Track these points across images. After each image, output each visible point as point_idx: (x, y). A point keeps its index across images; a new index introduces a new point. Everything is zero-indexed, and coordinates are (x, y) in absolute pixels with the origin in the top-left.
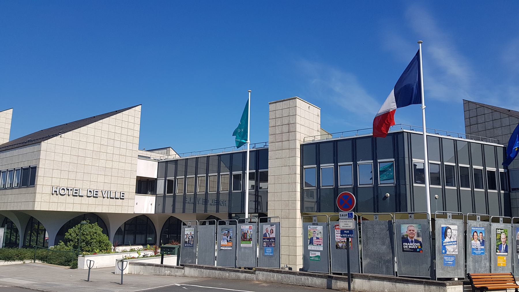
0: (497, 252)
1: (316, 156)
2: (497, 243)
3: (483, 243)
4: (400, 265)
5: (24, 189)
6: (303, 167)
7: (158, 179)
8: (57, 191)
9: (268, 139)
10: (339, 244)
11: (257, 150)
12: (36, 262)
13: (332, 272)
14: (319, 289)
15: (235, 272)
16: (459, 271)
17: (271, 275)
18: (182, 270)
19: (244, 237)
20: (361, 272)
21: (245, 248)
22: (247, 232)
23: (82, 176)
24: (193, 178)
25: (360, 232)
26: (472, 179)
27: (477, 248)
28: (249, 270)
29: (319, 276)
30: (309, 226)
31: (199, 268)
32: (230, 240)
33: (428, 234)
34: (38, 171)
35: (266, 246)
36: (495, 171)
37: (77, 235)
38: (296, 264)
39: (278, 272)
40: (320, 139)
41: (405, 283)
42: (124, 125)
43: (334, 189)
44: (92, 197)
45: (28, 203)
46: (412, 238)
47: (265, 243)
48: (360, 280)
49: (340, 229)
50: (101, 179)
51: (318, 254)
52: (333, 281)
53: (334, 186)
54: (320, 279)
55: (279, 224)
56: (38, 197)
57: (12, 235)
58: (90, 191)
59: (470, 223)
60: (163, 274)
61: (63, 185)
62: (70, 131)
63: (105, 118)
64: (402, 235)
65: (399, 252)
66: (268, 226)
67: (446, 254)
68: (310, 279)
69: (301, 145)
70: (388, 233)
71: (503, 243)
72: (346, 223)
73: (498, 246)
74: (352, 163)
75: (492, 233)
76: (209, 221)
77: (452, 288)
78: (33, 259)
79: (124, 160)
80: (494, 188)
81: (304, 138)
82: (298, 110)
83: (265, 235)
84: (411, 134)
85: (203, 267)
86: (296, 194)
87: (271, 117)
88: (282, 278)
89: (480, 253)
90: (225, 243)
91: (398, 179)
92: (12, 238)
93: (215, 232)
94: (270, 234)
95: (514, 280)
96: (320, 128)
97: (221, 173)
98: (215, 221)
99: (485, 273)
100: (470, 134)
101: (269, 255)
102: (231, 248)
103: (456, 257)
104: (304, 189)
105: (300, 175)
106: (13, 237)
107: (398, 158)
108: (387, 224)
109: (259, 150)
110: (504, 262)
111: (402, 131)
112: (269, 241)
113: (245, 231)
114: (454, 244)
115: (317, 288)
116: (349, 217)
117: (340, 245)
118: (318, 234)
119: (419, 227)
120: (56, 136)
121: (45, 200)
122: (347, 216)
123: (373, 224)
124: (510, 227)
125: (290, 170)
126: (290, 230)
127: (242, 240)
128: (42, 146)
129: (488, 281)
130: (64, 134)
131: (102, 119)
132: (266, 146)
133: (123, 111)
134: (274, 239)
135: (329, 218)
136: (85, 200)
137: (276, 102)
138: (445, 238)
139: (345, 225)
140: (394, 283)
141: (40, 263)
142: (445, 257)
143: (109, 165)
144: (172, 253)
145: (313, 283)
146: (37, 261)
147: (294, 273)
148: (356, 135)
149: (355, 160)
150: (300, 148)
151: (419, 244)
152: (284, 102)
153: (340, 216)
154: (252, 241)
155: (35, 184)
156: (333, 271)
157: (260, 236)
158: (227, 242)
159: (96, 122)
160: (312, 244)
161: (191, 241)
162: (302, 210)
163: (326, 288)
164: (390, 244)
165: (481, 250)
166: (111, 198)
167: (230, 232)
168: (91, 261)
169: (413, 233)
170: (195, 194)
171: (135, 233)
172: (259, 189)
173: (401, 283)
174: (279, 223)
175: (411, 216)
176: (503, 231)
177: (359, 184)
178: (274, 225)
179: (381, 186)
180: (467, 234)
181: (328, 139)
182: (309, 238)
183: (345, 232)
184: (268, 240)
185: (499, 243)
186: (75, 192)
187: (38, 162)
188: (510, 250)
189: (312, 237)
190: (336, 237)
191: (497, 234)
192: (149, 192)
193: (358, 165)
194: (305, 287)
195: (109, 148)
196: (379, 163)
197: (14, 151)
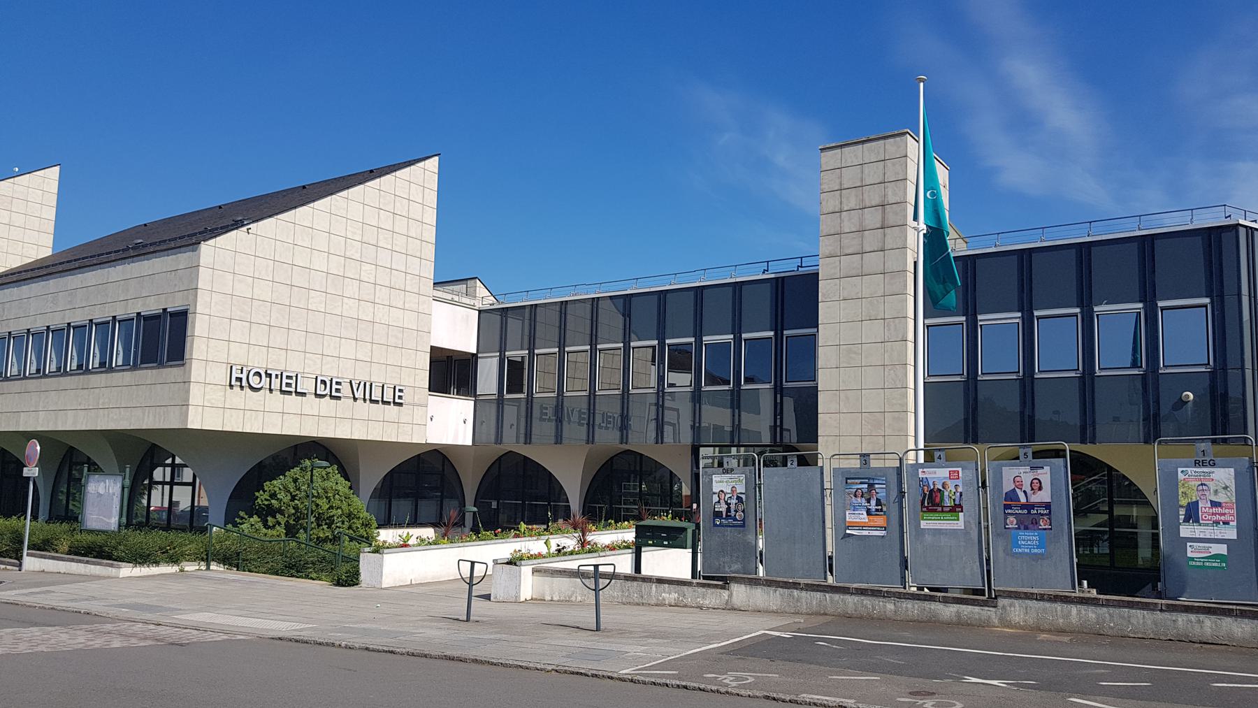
5: (150, 371)
7: (479, 355)
8: (241, 379)
9: (819, 245)
12: (212, 567)
15: (918, 600)
18: (722, 591)
22: (944, 488)
23: (303, 340)
24: (554, 355)
29: (1243, 615)
31: (781, 587)
32: (877, 510)
34: (194, 323)
35: (1016, 528)
37: (293, 498)
42: (401, 207)
43: (1022, 381)
44: (328, 398)
45: (165, 409)
50: (348, 350)
51: (1222, 549)
53: (1021, 374)
56: (196, 395)
57: (71, 498)
58: (324, 382)
60: (653, 601)
61: (256, 362)
62: (270, 216)
63: (355, 185)
66: (1022, 471)
68: (1182, 619)
74: (1077, 310)
76: (798, 456)
78: (202, 560)
79: (402, 303)
83: (1012, 496)
84: (1255, 232)
90: (864, 517)
92: (71, 507)
97: (599, 344)
98: (753, 456)
102: (882, 533)
106: (74, 503)
112: (1029, 513)
113: (934, 485)
120: (237, 228)
121: (213, 401)
125: (889, 330)
128: (202, 254)
130: (255, 225)
131: (348, 188)
132: (801, 267)
133: (395, 171)
134: (1047, 506)
136: (310, 403)
137: (841, 146)
141: (221, 572)
143: (366, 313)
144: (676, 543)
146: (214, 566)
149: (1085, 301)
154: (962, 511)
155: (187, 356)
158: (869, 512)
159: (332, 194)
161: (736, 511)
166: (372, 401)
167: (877, 486)
168: (473, 563)
170: (592, 396)
171: (416, 495)
172: (786, 382)
177: (1099, 369)
178: (1043, 468)
182: (1184, 502)
184: (1026, 512)
186: (287, 383)
187: (191, 298)
189: (1194, 500)
192: (454, 388)
193: (1097, 315)
195: (366, 267)
196: (1163, 309)
197: (110, 269)
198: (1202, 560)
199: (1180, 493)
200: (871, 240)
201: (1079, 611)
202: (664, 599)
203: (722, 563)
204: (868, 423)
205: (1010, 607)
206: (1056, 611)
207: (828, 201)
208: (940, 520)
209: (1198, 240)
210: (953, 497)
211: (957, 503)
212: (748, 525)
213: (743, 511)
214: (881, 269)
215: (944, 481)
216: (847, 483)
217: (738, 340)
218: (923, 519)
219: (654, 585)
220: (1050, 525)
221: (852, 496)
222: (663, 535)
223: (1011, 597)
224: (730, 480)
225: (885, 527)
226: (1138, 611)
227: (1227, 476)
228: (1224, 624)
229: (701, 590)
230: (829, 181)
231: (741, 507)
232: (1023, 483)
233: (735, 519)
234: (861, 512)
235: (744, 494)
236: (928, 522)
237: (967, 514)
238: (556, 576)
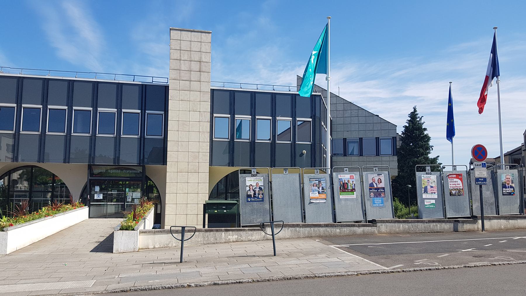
1: (231, 104)
10: (452, 191)
17: (396, 225)
21: (346, 200)
22: (348, 182)
31: (291, 227)
32: (322, 192)
35: (373, 197)
43: (250, 143)
51: (433, 201)
54: (448, 224)
60: (224, 241)
66: (375, 176)
72: (481, 172)
74: (271, 118)
85: (300, 225)
88: (409, 228)
90: (317, 195)
94: (377, 183)
98: (417, 166)
102: (325, 201)
104: (213, 140)
112: (378, 191)
116: (482, 167)
118: (432, 183)
122: (481, 166)
127: (341, 191)
134: (384, 188)
137: (181, 30)
139: (480, 174)
140: (508, 220)
149: (274, 115)
152: (193, 33)
154: (355, 191)
158: (319, 193)
161: (259, 194)
164: (493, 190)
167: (322, 182)
172: (147, 135)
173: (513, 219)
182: (423, 186)
183: (480, 179)
184: (376, 191)
189: (426, 186)
190: (450, 186)
199: (422, 183)
200: (194, 76)
202: (229, 239)
203: (252, 219)
204: (191, 156)
205: (381, 226)
208: (347, 195)
210: (352, 186)
211: (353, 188)
212: (265, 201)
213: (263, 194)
214: (199, 89)
215: (348, 179)
217: (19, 107)
218: (341, 195)
219: (223, 233)
220: (385, 195)
221: (312, 186)
222: (223, 207)
224: (255, 180)
225: (325, 199)
226: (420, 224)
228: (443, 225)
229: (250, 232)
230: (174, 45)
231: (261, 192)
232: (375, 180)
233: (258, 198)
235: (263, 186)
236: (343, 196)
237: (357, 192)
238: (157, 234)
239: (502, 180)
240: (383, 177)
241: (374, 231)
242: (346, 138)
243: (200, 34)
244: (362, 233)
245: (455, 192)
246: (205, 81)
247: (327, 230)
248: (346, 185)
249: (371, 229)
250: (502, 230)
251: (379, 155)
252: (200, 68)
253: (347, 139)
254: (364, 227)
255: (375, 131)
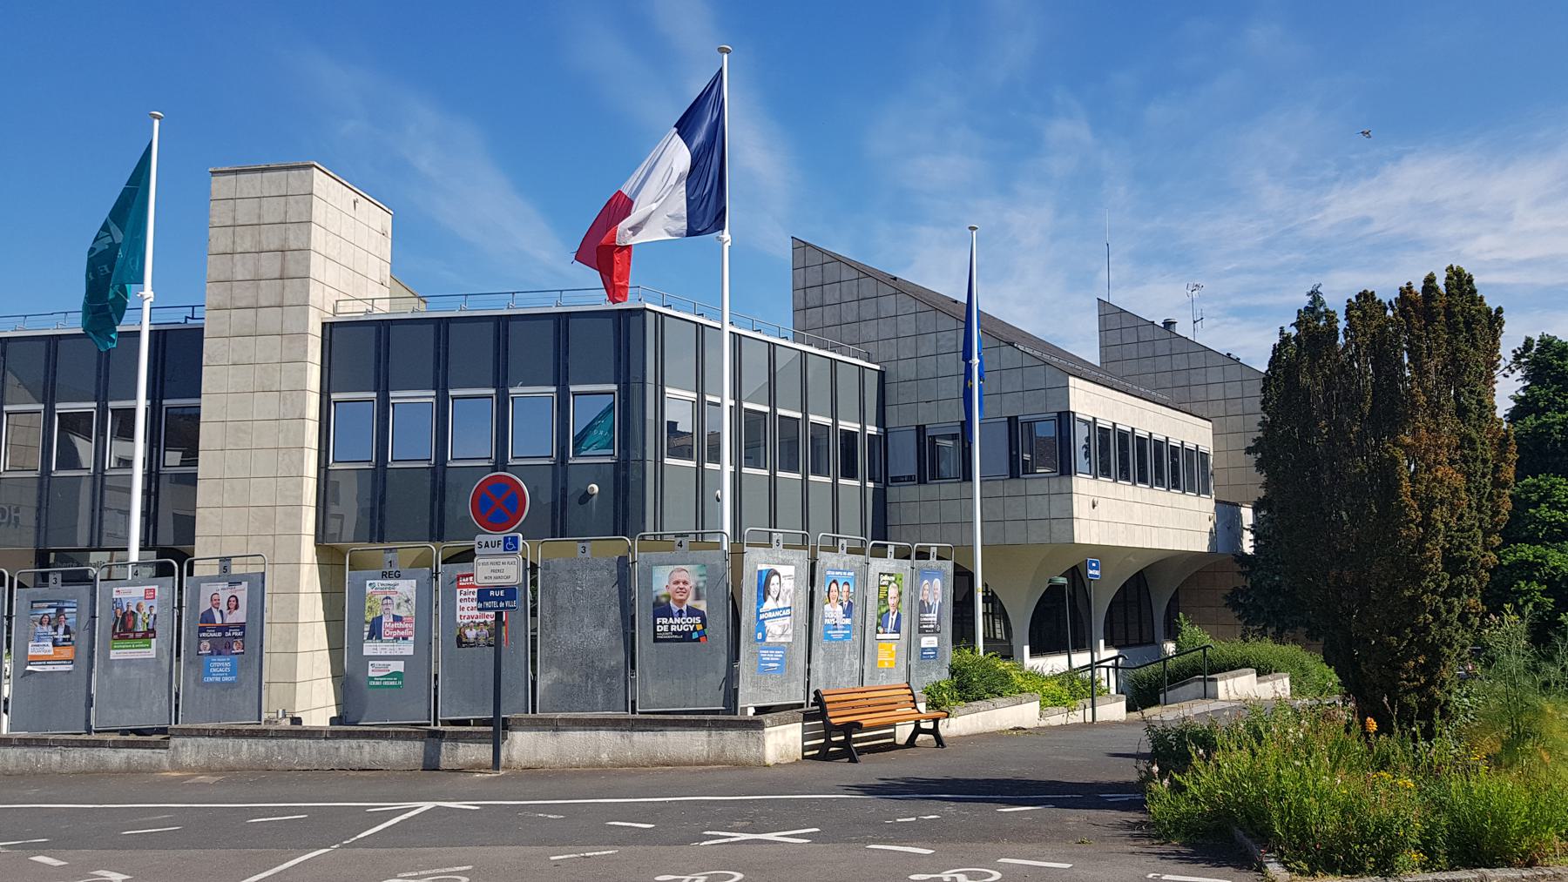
0: (878, 632)
2: (880, 608)
3: (848, 612)
4: (646, 682)
6: (329, 396)
11: (158, 331)
13: (440, 718)
14: (399, 773)
15: (87, 746)
16: (793, 686)
17: (228, 745)
19: (125, 627)
20: (530, 712)
22: (138, 610)
25: (534, 592)
26: (804, 451)
27: (836, 624)
28: (141, 736)
29: (398, 736)
30: (368, 582)
32: (64, 640)
33: (723, 588)
35: (210, 654)
36: (857, 430)
38: (294, 709)
39: (254, 734)
40: (386, 309)
41: (659, 729)
43: (433, 470)
46: (681, 602)
47: (206, 643)
48: (529, 733)
49: (476, 587)
51: (399, 666)
52: (445, 746)
55: (260, 578)
59: (825, 558)
64: (654, 595)
65: (643, 644)
66: (220, 587)
67: (764, 643)
68: (367, 746)
69: (324, 324)
70: (617, 592)
71: (892, 610)
72: (496, 567)
73: (880, 616)
74: (492, 391)
75: (870, 585)
77: (776, 732)
80: (853, 476)
81: (337, 301)
82: (317, 207)
83: (208, 617)
86: (300, 486)
87: (215, 221)
89: (840, 637)
90: (48, 649)
91: (625, 444)
93: (3, 613)
94: (225, 611)
95: (914, 701)
96: (388, 274)
99: (849, 688)
100: (805, 331)
101: (221, 682)
102: (70, 667)
103: (785, 648)
104: (330, 468)
105: (317, 423)
107: (627, 383)
108: (615, 568)
109: (166, 330)
110: (891, 657)
111: (640, 306)
112: (223, 635)
114: (784, 616)
115: (390, 773)
116: (505, 550)
117: (471, 634)
118: (399, 605)
119: (701, 573)
122: (502, 546)
123: (575, 568)
124: (909, 567)
126: (276, 602)
127: (116, 637)
129: (858, 707)
132: (193, 318)
134: (242, 627)
135: (437, 555)
137: (236, 172)
138: (765, 600)
140: (628, 733)
142: (761, 652)
145: (379, 758)
147: (313, 734)
148: (508, 308)
149: (501, 383)
150: (320, 335)
151: (698, 620)
152: (267, 175)
153: (477, 546)
154: (155, 637)
156: (443, 715)
157: (188, 622)
158: (55, 643)
160: (379, 638)
162: (320, 538)
163: (421, 768)
164: (620, 624)
165: (843, 630)
167: (66, 610)
169: (684, 590)
172: (164, 466)
174: (260, 576)
175: (681, 542)
176: (893, 578)
179: (575, 462)
180: (815, 589)
181: (419, 311)
182: (369, 618)
183: (492, 593)
184: (220, 634)
185: (884, 610)
188: (904, 627)
190: (459, 613)
191: (880, 586)
193: (513, 398)
194: (352, 773)
196: (575, 394)
198: (381, 679)
200: (268, 293)
201: (250, 745)
204: (256, 519)
206: (227, 748)
207: (217, 239)
208: (132, 648)
209: (610, 322)
210: (147, 621)
211: (150, 627)
214: (277, 329)
215: (138, 601)
216: (32, 607)
223: (184, 736)
225: (72, 661)
226: (305, 741)
227: (410, 588)
234: (46, 643)
236: (118, 651)
237: (160, 640)
239: (655, 587)
240: (243, 590)
241: (160, 760)
242: (924, 426)
243: (284, 173)
244: (124, 766)
245: (477, 634)
246: (295, 303)
247: (25, 757)
248: (132, 618)
249: (152, 755)
250: (600, 766)
251: (1018, 477)
252: (283, 269)
253: (927, 427)
254: (132, 750)
255: (1005, 397)
